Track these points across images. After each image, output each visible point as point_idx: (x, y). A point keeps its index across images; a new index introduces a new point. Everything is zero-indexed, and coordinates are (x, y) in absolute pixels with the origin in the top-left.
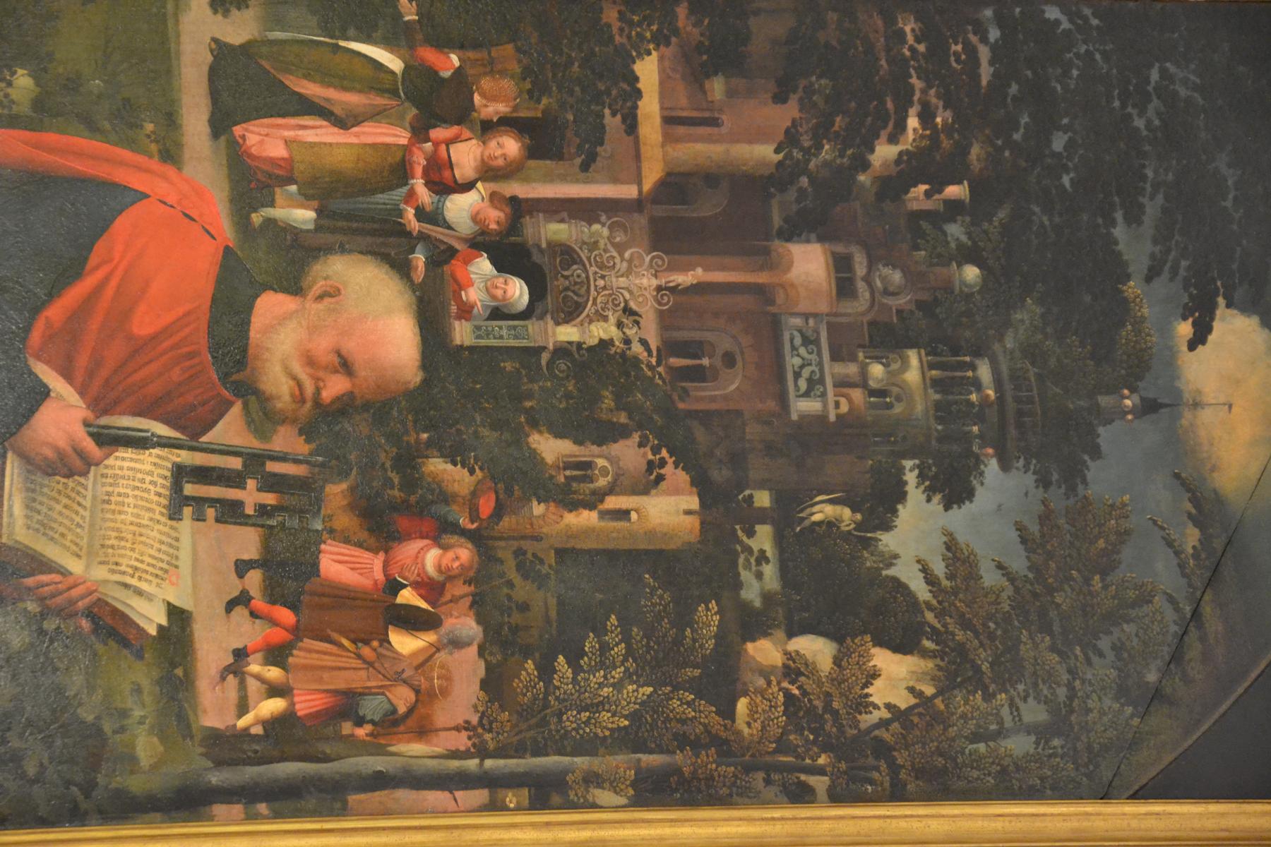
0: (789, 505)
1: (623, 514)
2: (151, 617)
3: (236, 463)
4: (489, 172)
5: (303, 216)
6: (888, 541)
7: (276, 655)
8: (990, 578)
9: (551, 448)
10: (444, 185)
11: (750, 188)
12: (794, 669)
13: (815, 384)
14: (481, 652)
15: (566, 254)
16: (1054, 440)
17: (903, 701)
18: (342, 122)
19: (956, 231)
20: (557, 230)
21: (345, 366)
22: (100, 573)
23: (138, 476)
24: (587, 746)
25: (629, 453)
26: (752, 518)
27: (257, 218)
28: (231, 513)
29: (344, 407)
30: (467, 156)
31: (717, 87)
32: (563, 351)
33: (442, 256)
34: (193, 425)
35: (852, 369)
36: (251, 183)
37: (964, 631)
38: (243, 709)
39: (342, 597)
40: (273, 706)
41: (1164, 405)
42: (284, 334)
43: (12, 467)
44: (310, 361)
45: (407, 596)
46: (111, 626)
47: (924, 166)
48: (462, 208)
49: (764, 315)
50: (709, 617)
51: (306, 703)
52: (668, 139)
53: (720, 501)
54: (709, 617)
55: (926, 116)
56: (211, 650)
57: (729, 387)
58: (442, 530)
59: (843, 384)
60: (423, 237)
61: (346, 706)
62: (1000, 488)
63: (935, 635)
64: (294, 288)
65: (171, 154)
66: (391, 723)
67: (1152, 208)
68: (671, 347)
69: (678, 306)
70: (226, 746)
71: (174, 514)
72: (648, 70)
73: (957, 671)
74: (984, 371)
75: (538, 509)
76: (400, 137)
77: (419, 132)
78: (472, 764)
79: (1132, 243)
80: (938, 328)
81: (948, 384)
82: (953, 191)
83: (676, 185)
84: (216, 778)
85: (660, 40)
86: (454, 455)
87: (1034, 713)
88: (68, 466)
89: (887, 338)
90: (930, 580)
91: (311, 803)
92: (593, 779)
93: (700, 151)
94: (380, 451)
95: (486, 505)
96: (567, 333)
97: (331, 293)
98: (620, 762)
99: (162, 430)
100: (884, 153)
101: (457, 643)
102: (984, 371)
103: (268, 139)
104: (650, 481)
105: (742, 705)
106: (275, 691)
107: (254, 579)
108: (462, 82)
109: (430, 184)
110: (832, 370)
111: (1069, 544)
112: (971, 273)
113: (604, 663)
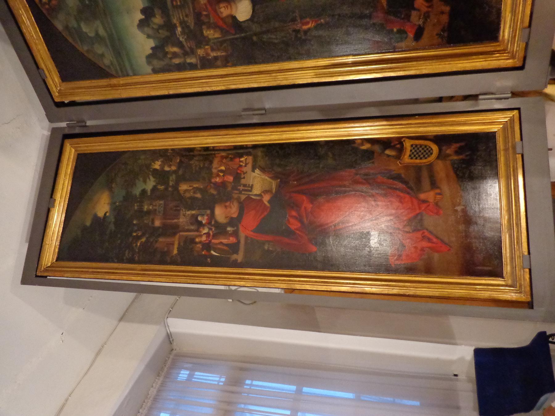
0: (166, 189)
1: (190, 186)
2: (257, 171)
3: (243, 192)
4: (201, 236)
5: (229, 229)
6: (154, 184)
7: (241, 166)
8: (141, 179)
9: (198, 195)
10: (208, 234)
11: (163, 234)
12: (170, 166)
13: (160, 205)
14: (212, 167)
15: (192, 224)
16: (128, 198)
17: (157, 162)
18: (221, 243)
19: (136, 228)
20: (192, 227)
21: (226, 207)
22: (263, 177)
23: (256, 191)
24: (200, 155)
25: (188, 195)
26: (173, 186)
27: (236, 228)
28: (245, 186)
29: (226, 201)
30: (204, 238)
31: (166, 249)
32: (194, 209)
33: (209, 223)
34: (249, 198)
35: (154, 208)
36: (235, 234)
37: (145, 171)
38: (246, 159)
39: (230, 174)
40: (242, 159)
41: (112, 204)
42: (234, 211)
43: (274, 191)
44: (231, 207)
45: (221, 174)
46: (263, 170)
47: (138, 238)
48: (206, 231)
49: (165, 216)
50: (180, 172)
51: (237, 160)
52: (174, 242)
53: (176, 188)
54: (180, 172)
55: (136, 245)
56: (250, 166)
57: (172, 204)
58: (215, 184)
59: (155, 206)
60: (212, 226)
61: (232, 159)
62: (137, 191)
63: (150, 171)
64: (232, 218)
65: (246, 238)
66: (226, 157)
67: (108, 232)
68: (179, 211)
69: (177, 216)
70: (248, 154)
71: (252, 185)
72: (175, 252)
73: (148, 166)
74: (136, 208)
75: (202, 187)
76: (213, 241)
77: (210, 242)
78: (216, 152)
79: (112, 227)
80: (141, 214)
81: (141, 206)
82: (135, 234)
83: (174, 234)
84: (251, 150)
85: (172, 256)
86: (213, 195)
87: (140, 161)
88: (265, 192)
89: (149, 212)
90: (149, 178)
91: (232, 147)
92: (200, 151)
93: (169, 240)
94: (224, 195)
95: (209, 187)
96: (193, 212)
97: (226, 217)
98: (196, 153)
99: (253, 197)
100: (144, 240)
101: (216, 168)
102: (136, 208)
103: (232, 240)
104: (186, 191)
105: (178, 161)
106: (242, 161)
107: (242, 176)
108: (203, 249)
109: (210, 234)
110: (157, 208)
111: (130, 184)
112: (135, 222)
113: (196, 166)
